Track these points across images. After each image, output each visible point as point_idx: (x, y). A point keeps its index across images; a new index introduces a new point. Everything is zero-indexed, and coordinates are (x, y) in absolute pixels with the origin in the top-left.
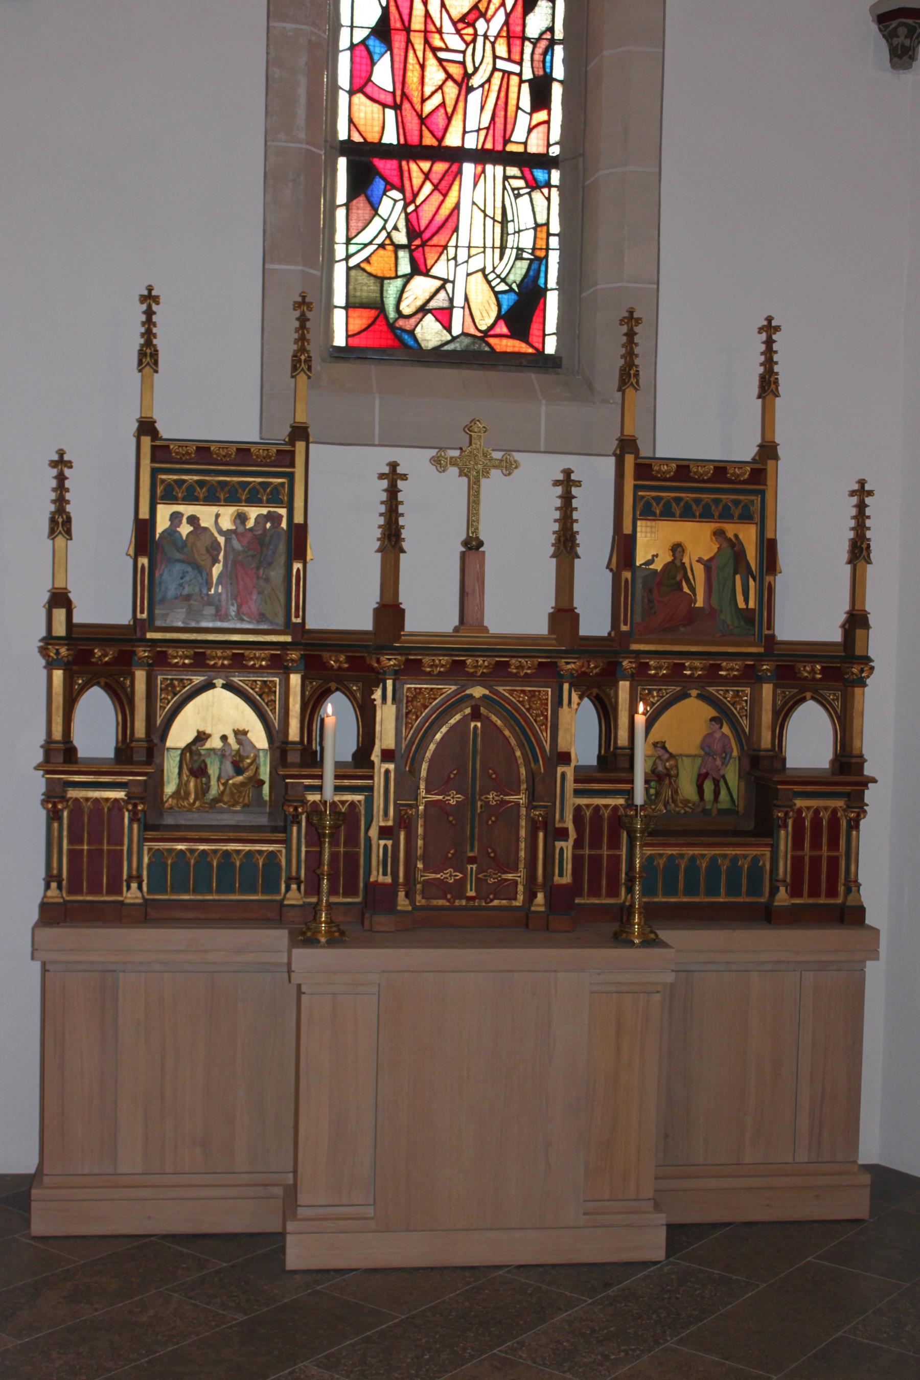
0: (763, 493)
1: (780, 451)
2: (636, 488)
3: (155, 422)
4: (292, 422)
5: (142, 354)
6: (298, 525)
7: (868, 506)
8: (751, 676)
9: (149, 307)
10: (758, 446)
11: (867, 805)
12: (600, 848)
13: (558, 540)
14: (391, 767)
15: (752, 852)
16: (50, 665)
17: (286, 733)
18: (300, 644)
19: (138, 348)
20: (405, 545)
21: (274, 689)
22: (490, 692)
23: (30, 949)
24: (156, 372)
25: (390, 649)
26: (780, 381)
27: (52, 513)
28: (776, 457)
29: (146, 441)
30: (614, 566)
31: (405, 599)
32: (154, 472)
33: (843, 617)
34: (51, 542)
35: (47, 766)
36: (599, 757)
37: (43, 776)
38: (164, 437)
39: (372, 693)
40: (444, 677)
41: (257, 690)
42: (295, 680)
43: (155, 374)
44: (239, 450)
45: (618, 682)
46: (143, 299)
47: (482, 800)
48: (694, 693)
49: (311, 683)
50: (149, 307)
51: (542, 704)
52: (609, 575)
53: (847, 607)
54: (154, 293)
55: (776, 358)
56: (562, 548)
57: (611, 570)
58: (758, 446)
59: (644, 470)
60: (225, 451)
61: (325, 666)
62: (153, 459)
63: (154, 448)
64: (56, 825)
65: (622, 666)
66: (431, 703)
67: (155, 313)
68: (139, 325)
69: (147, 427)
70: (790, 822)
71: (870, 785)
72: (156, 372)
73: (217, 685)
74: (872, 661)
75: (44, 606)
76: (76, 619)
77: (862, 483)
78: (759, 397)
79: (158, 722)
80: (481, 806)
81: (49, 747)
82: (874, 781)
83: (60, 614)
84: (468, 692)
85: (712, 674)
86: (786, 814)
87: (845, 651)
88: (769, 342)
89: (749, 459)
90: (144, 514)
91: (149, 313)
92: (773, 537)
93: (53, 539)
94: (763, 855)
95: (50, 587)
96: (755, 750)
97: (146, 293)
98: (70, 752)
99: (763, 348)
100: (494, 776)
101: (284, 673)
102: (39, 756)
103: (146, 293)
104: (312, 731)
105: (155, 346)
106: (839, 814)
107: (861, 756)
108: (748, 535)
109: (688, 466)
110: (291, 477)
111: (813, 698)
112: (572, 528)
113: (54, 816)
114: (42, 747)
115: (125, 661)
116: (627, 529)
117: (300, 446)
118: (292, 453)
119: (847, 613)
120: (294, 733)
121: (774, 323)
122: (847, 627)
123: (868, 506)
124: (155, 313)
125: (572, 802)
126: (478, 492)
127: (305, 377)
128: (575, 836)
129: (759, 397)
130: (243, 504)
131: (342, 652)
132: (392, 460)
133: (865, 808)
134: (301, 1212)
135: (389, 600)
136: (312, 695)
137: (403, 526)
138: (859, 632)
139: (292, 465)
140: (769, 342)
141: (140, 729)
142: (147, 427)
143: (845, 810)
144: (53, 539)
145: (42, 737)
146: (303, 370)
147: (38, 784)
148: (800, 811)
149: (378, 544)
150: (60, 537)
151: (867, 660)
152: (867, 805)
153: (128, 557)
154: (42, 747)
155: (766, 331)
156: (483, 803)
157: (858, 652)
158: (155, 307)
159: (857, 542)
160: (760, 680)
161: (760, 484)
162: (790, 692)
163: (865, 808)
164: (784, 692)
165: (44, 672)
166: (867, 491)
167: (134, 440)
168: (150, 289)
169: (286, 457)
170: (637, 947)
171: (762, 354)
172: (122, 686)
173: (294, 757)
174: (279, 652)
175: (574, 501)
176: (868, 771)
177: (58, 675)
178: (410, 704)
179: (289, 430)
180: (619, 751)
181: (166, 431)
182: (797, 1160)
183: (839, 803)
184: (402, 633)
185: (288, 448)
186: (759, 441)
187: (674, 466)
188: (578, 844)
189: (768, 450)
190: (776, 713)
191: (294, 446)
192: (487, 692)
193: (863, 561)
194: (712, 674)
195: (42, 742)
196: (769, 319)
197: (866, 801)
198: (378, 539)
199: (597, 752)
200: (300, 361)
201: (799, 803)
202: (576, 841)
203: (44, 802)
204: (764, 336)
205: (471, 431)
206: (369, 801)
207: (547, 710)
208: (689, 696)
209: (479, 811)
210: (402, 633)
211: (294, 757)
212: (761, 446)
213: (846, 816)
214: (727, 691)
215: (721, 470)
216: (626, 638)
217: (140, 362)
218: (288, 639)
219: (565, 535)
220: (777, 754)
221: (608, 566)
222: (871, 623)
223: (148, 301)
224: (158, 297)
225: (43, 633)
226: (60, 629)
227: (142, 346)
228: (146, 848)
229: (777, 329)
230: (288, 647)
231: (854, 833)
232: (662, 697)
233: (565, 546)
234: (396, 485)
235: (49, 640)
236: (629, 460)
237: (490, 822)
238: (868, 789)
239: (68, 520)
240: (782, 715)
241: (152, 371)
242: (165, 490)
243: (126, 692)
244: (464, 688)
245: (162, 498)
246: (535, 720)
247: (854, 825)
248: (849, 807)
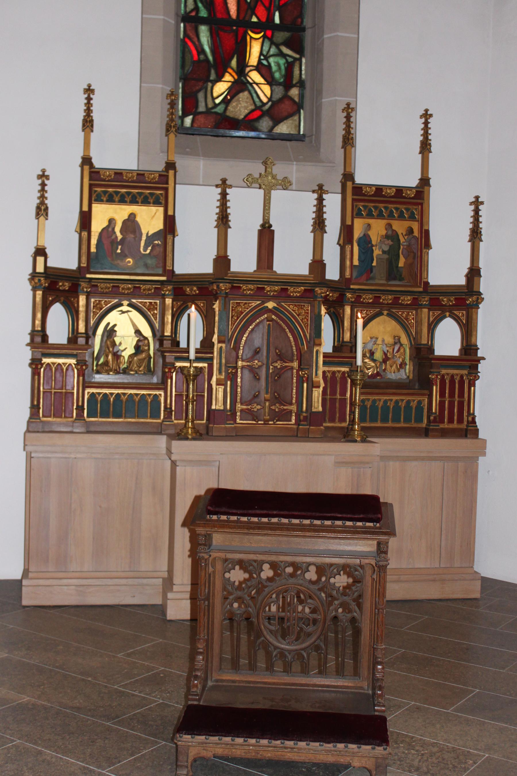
0: (422, 204)
1: (431, 182)
2: (354, 200)
3: (46, 248)
4: (166, 160)
5: (38, 208)
6: (170, 216)
7: (480, 210)
8: (416, 305)
9: (89, 96)
10: (419, 180)
11: (480, 372)
12: (336, 395)
13: (315, 223)
14: (223, 345)
15: (418, 398)
16: (34, 289)
17: (163, 332)
18: (171, 282)
19: (82, 118)
20: (231, 224)
21: (156, 306)
22: (277, 305)
23: (22, 445)
24: (47, 219)
25: (222, 279)
26: (432, 144)
27: (38, 204)
28: (429, 186)
29: (86, 168)
30: (341, 242)
31: (230, 253)
32: (91, 186)
33: (466, 271)
34: (37, 221)
35: (32, 344)
36: (334, 347)
37: (30, 350)
38: (96, 167)
39: (214, 304)
40: (252, 297)
41: (147, 307)
42: (169, 301)
43: (47, 221)
44: (138, 174)
45: (344, 306)
46: (40, 177)
47: (272, 366)
48: (385, 312)
49: (177, 303)
50: (89, 96)
51: (305, 313)
52: (338, 248)
53: (468, 265)
54: (46, 174)
55: (430, 131)
56: (317, 227)
57: (340, 245)
58: (419, 180)
59: (358, 189)
60: (131, 175)
61: (183, 293)
62: (91, 179)
63: (91, 173)
64: (36, 377)
65: (346, 296)
66: (245, 311)
67: (46, 185)
68: (83, 105)
69: (87, 161)
70: (438, 381)
71: (481, 361)
72: (47, 219)
73: (124, 304)
74: (482, 294)
75: (32, 256)
76: (49, 264)
77: (477, 198)
78: (420, 153)
79: (92, 324)
80: (272, 368)
81: (33, 333)
82: (483, 358)
83: (40, 260)
84: (266, 305)
85: (396, 303)
86: (437, 376)
87: (467, 289)
88: (426, 123)
89: (414, 186)
90: (85, 208)
91: (43, 185)
92: (427, 228)
93: (38, 219)
94: (424, 400)
95: (35, 245)
96: (418, 345)
97: (87, 88)
98: (45, 337)
99: (423, 126)
100: (279, 353)
101: (162, 298)
102: (28, 340)
103: (41, 173)
104: (177, 328)
105: (46, 204)
106: (464, 378)
107: (477, 346)
108: (415, 226)
109: (382, 189)
110: (166, 190)
111: (450, 316)
112: (323, 216)
113: (35, 373)
114: (29, 334)
115: (74, 291)
116: (349, 222)
117: (171, 173)
118: (167, 176)
119: (469, 268)
120: (168, 333)
121: (429, 113)
122: (469, 276)
123: (480, 210)
124: (46, 185)
125: (321, 368)
126: (270, 197)
127: (174, 136)
128: (324, 385)
129: (420, 153)
130: (140, 204)
131: (195, 285)
132: (224, 177)
133: (479, 374)
134: (175, 588)
135: (222, 254)
136: (176, 311)
137: (229, 213)
138: (476, 279)
139: (167, 183)
140: (426, 123)
141: (82, 328)
142: (87, 161)
143: (467, 375)
144: (38, 219)
145: (29, 329)
146: (172, 131)
147: (27, 354)
148: (443, 376)
149: (215, 223)
150: (42, 217)
151: (480, 294)
152: (480, 372)
153: (76, 233)
154: (29, 334)
155: (424, 117)
156: (273, 367)
157: (475, 290)
158: (46, 182)
159: (474, 229)
160: (422, 306)
161: (420, 199)
162: (437, 313)
163: (479, 374)
164: (434, 313)
165: (31, 293)
166: (480, 202)
167: (79, 169)
168: (44, 171)
169: (163, 178)
170: (359, 443)
171: (422, 129)
172: (72, 304)
173: (167, 344)
174: (159, 286)
175: (324, 201)
176: (480, 354)
177: (39, 293)
178: (233, 311)
179: (164, 165)
180: (344, 344)
181: (97, 163)
182: (441, 566)
183: (465, 372)
184: (229, 272)
185: (165, 173)
186: (420, 177)
187: (374, 188)
188: (324, 392)
189: (425, 182)
190: (429, 325)
191: (168, 172)
192: (275, 305)
193: (478, 240)
194: (396, 303)
195: (29, 331)
196: (427, 111)
197: (479, 370)
198: (216, 221)
199: (332, 345)
200: (171, 126)
201: (444, 371)
202: (324, 388)
203: (30, 365)
204: (423, 120)
205: (266, 164)
206: (211, 366)
207: (308, 316)
208: (383, 314)
209: (271, 371)
210: (229, 272)
211: (167, 344)
212: (421, 180)
213: (468, 379)
214: (404, 312)
215: (399, 190)
216: (349, 281)
217: (84, 125)
218: (164, 278)
219: (319, 220)
220: (431, 349)
221: (338, 243)
222: (482, 274)
223: (43, 179)
224: (48, 176)
225: (30, 271)
226: (40, 269)
227: (85, 116)
228: (86, 392)
229: (431, 115)
230: (165, 283)
231: (472, 388)
232: (368, 315)
233: (319, 226)
234: (226, 191)
235: (34, 275)
236: (349, 184)
237: (276, 378)
238: (480, 363)
239: (47, 209)
240: (432, 327)
241: (44, 219)
242: (97, 196)
243: (74, 306)
244: (263, 303)
245: (96, 200)
246: (302, 321)
247: (472, 384)
248: (470, 374)
